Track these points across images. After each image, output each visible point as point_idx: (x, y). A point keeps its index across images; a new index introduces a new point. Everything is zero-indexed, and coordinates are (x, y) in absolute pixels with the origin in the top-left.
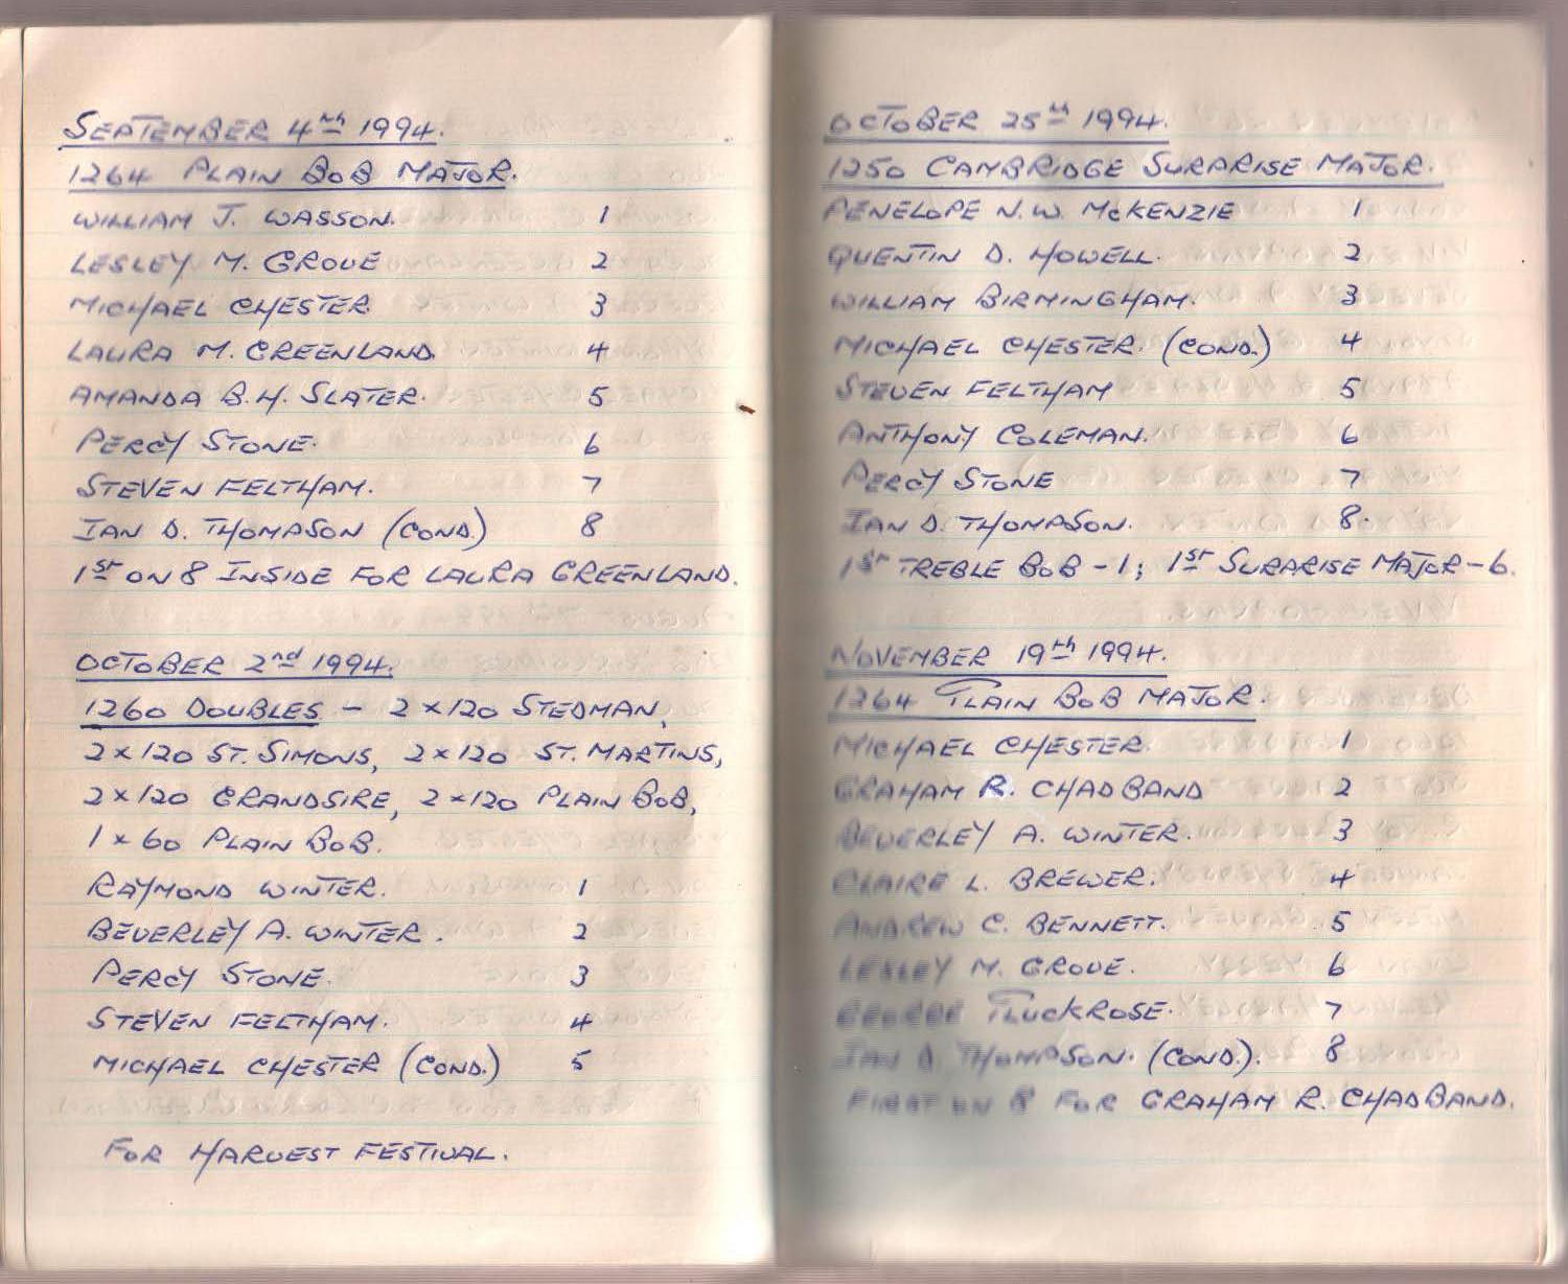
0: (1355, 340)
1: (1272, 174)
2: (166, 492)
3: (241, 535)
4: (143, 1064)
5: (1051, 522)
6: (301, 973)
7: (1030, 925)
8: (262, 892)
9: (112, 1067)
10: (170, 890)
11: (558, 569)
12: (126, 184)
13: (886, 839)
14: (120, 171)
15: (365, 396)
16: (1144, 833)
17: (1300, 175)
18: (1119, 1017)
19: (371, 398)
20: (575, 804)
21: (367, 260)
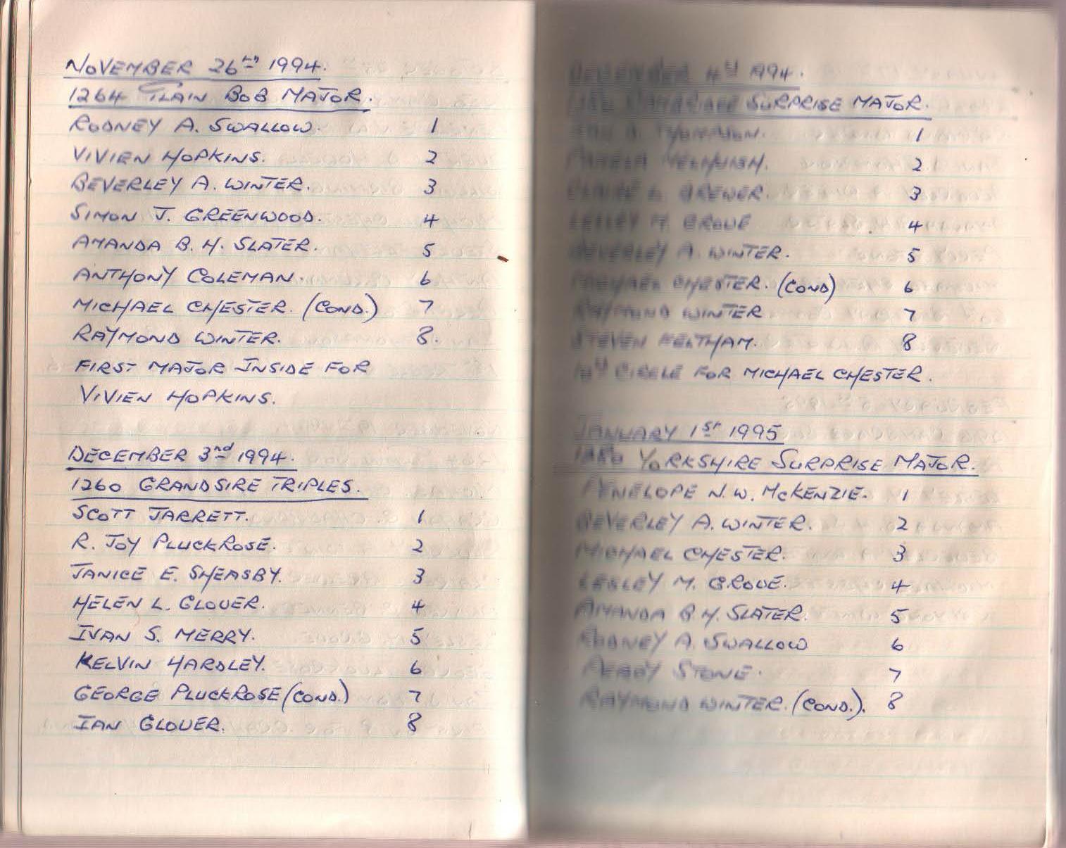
0: (432, 220)
2: (129, 400)
4: (141, 693)
6: (221, 302)
7: (74, 184)
11: (192, 211)
12: (107, 102)
13: (730, 223)
14: (103, 92)
15: (765, 612)
16: (758, 252)
18: (143, 342)
19: (769, 614)
20: (92, 339)
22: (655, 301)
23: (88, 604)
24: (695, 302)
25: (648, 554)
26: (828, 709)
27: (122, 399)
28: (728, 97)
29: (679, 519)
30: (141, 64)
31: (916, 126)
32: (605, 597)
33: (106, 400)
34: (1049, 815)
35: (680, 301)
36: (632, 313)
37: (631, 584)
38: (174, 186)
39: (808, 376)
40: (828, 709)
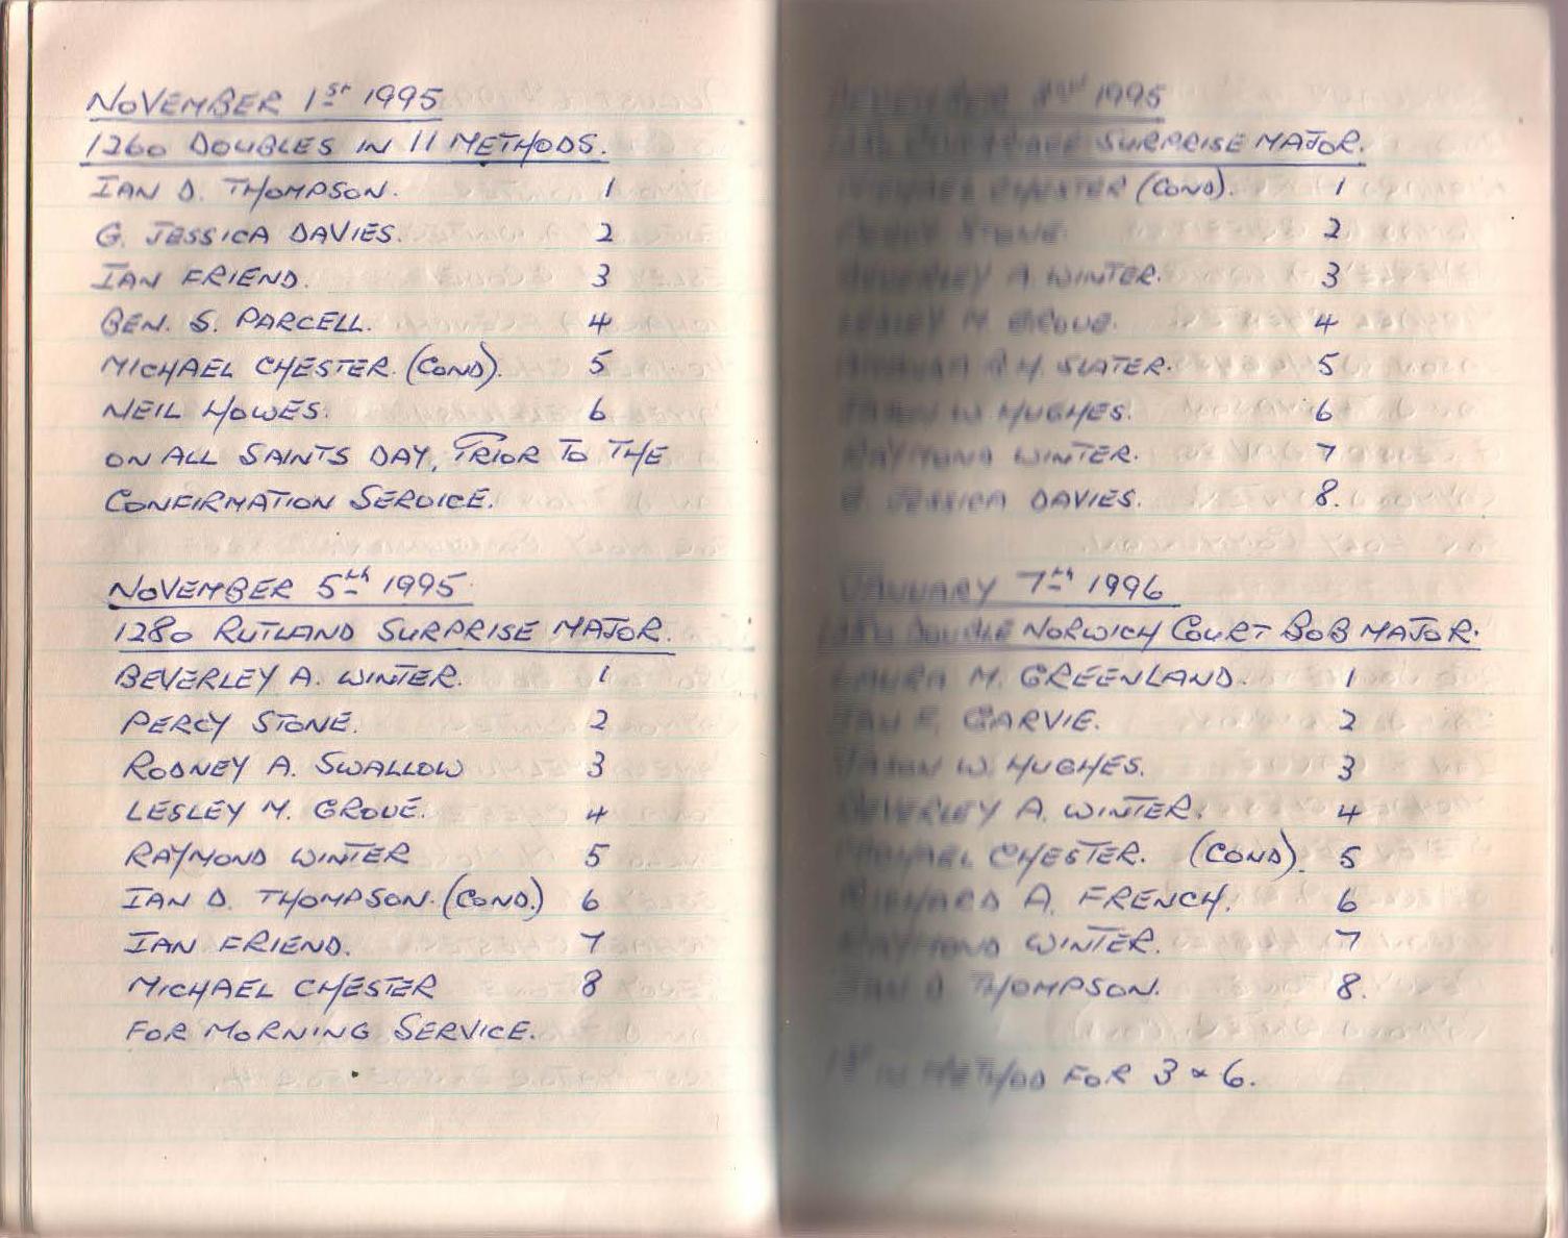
1: (336, 197)
5: (312, 190)
8: (294, 861)
9: (298, 195)
10: (153, 985)
13: (1082, 322)
21: (286, 409)
22: (968, 440)
24: (1031, 437)
27: (359, 235)
28: (1066, 133)
30: (205, 100)
31: (1338, 174)
34: (1552, 1194)
35: (1003, 442)
36: (941, 461)
38: (147, 936)
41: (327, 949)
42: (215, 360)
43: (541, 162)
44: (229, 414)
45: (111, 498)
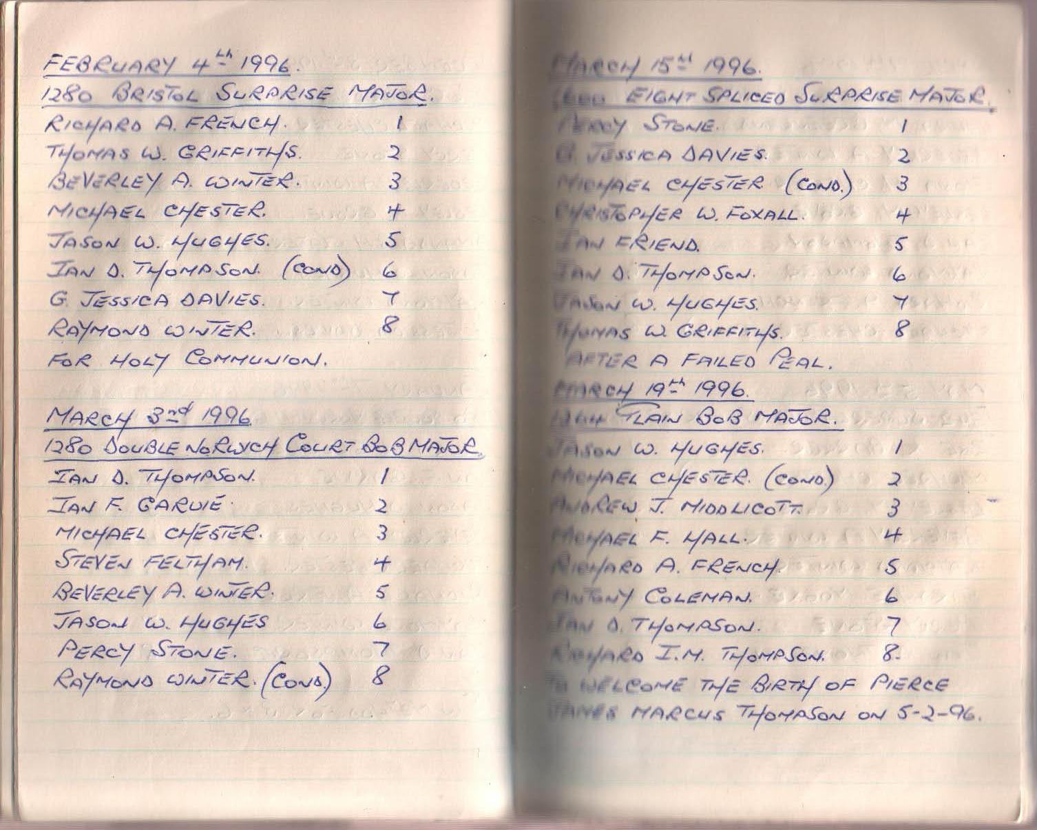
3: (130, 363)
17: (906, 102)
23: (194, 534)
25: (615, 479)
26: (833, 718)
27: (736, 157)
29: (694, 566)
32: (585, 290)
33: (719, 158)
37: (129, 182)
39: (734, 689)
40: (833, 718)
41: (142, 683)
42: (71, 57)
43: (660, 430)
44: (71, 155)
45: (655, 475)
